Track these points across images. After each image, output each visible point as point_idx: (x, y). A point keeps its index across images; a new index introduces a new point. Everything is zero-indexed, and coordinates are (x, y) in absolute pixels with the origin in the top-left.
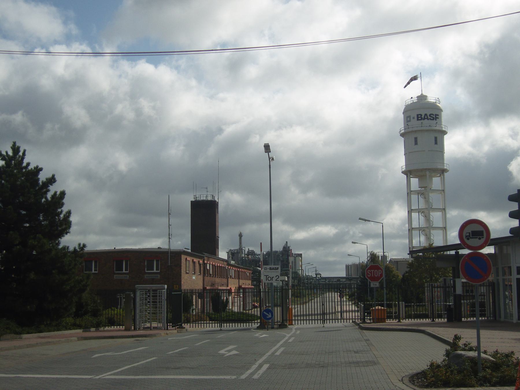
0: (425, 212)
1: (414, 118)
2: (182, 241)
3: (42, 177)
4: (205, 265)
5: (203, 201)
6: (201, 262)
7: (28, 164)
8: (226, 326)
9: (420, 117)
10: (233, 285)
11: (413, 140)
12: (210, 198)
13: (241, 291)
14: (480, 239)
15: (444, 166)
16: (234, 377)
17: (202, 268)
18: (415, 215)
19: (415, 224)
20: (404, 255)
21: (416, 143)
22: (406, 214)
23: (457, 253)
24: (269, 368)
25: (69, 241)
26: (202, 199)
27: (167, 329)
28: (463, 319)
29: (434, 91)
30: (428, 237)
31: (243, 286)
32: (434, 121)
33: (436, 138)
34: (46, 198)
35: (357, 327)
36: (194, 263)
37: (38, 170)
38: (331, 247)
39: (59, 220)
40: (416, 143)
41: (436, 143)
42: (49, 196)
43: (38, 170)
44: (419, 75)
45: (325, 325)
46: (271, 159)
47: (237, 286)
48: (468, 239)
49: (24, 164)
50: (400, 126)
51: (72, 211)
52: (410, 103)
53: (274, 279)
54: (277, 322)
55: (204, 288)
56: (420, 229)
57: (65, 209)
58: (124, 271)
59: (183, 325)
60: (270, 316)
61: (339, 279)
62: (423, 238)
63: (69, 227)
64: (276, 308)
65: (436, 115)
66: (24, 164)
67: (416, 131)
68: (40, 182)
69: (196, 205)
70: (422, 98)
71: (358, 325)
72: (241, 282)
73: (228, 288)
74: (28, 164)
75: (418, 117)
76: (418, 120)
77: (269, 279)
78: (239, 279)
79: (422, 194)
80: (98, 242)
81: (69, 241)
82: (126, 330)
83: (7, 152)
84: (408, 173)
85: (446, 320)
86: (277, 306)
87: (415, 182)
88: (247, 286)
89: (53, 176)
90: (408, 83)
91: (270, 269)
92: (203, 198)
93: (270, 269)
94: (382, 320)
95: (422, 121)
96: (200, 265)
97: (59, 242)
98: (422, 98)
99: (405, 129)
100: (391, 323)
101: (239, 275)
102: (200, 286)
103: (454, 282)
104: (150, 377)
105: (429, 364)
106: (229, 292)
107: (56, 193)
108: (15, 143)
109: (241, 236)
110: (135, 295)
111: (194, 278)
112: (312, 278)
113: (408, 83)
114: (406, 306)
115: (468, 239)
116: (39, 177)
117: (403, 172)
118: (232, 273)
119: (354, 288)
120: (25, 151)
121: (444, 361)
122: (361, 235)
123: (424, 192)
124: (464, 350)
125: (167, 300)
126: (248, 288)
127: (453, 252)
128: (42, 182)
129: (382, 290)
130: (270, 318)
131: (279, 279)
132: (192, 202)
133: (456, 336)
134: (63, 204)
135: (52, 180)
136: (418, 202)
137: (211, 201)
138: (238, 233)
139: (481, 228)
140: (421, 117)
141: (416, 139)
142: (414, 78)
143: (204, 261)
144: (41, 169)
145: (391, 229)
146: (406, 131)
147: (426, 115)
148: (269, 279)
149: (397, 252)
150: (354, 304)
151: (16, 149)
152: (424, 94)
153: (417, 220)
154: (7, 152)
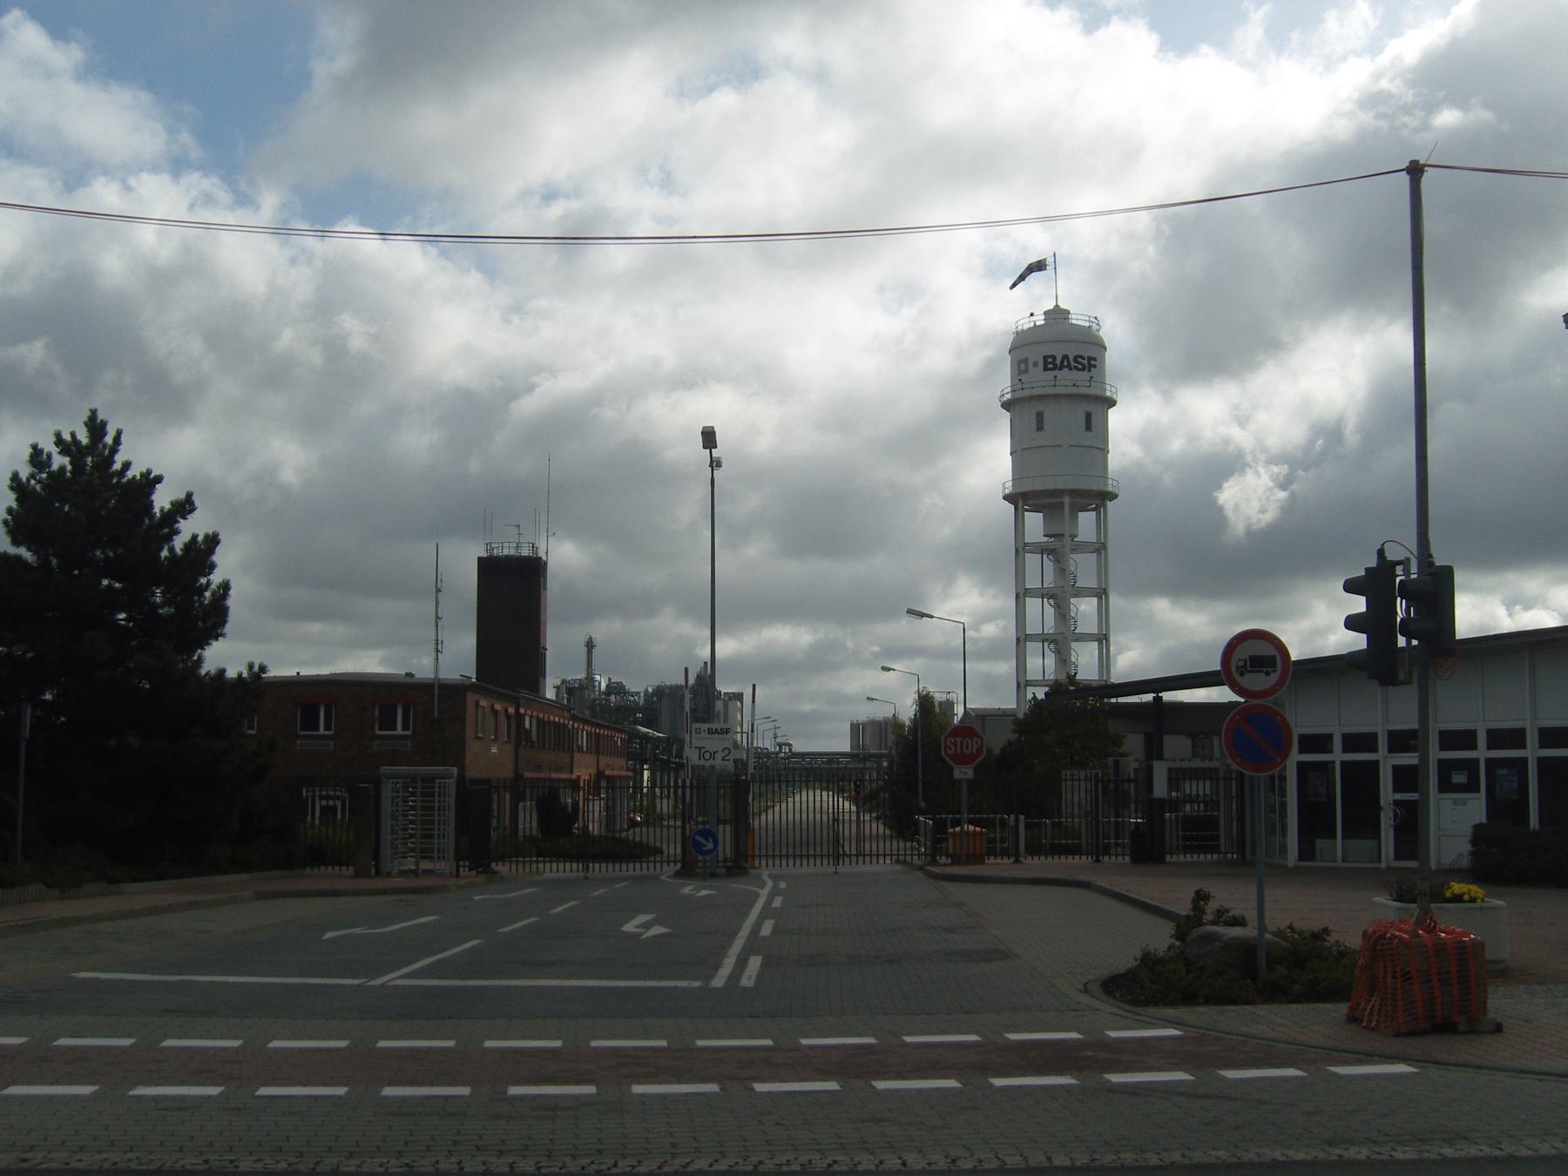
0: (1059, 597)
1: (1035, 364)
2: (459, 655)
3: (162, 500)
4: (520, 717)
5: (508, 558)
6: (511, 710)
7: (127, 466)
8: (598, 869)
9: (1050, 363)
10: (584, 770)
11: (1034, 416)
12: (525, 552)
13: (603, 784)
14: (1268, 674)
15: (1106, 484)
16: (696, 984)
17: (513, 727)
18: (1033, 605)
19: (1033, 627)
20: (1006, 700)
21: (1040, 427)
22: (1011, 603)
23: (1158, 700)
24: (764, 965)
25: (224, 656)
26: (506, 552)
27: (458, 875)
28: (1168, 858)
29: (1071, 294)
30: (1063, 659)
31: (608, 773)
32: (1085, 375)
33: (1088, 416)
34: (172, 550)
35: (919, 874)
36: (495, 712)
37: (150, 482)
38: (820, 683)
39: (201, 603)
40: (1040, 427)
41: (1088, 427)
42: (179, 543)
43: (150, 482)
44: (1050, 261)
45: (841, 869)
46: (715, 464)
47: (593, 771)
48: (1242, 674)
49: (117, 466)
50: (1003, 383)
51: (232, 584)
52: (1026, 327)
53: (719, 756)
54: (725, 861)
55: (518, 777)
56: (1043, 638)
57: (216, 578)
58: (322, 731)
59: (493, 865)
60: (710, 846)
61: (832, 757)
62: (1050, 661)
63: (224, 622)
64: (721, 828)
65: (1090, 359)
66: (117, 466)
67: (1040, 398)
68: (157, 510)
69: (490, 568)
70: (1057, 315)
71: (921, 868)
72: (604, 761)
73: (574, 776)
74: (127, 466)
75: (1046, 363)
76: (1046, 369)
77: (707, 756)
78: (598, 754)
79: (1051, 552)
80: (290, 662)
81: (224, 656)
82: (357, 876)
83: (73, 435)
84: (1019, 499)
85: (1127, 859)
86: (725, 822)
87: (1035, 522)
88: (615, 773)
89: (189, 495)
90: (1022, 278)
91: (710, 731)
92: (508, 551)
93: (710, 731)
94: (977, 859)
95: (1056, 372)
96: (508, 717)
97: (200, 657)
98: (1057, 315)
99: (1013, 391)
100: (998, 865)
101: (598, 745)
102: (505, 771)
103: (1150, 770)
104: (498, 983)
105: (1139, 954)
106: (574, 785)
107: (195, 537)
108: (94, 413)
109: (590, 645)
110: (378, 790)
111: (494, 750)
112: (768, 755)
113: (1022, 278)
114: (1028, 826)
115: (1242, 674)
116: (154, 497)
117: (1006, 498)
118: (583, 740)
119: (871, 781)
120: (119, 433)
121: (1171, 947)
122: (876, 649)
123: (1056, 548)
124: (1213, 923)
125: (1379, 809)
126: (620, 777)
127: (1149, 697)
128: (162, 510)
129: (953, 785)
130: (710, 852)
131: (731, 757)
132: (480, 559)
133: (1198, 892)
134: (213, 567)
135: (184, 507)
136: (1038, 571)
137: (528, 559)
138: (582, 641)
139: (1268, 650)
140: (1053, 363)
141: (1040, 416)
142: (1039, 266)
143: (517, 710)
144: (159, 479)
145: (962, 641)
146: (1018, 395)
147: (1065, 357)
148: (707, 756)
149: (990, 689)
150: (878, 818)
151: (96, 427)
152: (1063, 306)
153: (1040, 615)
154: (73, 435)
